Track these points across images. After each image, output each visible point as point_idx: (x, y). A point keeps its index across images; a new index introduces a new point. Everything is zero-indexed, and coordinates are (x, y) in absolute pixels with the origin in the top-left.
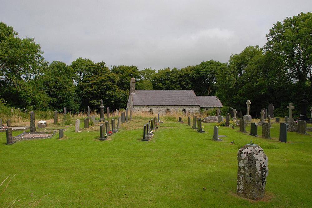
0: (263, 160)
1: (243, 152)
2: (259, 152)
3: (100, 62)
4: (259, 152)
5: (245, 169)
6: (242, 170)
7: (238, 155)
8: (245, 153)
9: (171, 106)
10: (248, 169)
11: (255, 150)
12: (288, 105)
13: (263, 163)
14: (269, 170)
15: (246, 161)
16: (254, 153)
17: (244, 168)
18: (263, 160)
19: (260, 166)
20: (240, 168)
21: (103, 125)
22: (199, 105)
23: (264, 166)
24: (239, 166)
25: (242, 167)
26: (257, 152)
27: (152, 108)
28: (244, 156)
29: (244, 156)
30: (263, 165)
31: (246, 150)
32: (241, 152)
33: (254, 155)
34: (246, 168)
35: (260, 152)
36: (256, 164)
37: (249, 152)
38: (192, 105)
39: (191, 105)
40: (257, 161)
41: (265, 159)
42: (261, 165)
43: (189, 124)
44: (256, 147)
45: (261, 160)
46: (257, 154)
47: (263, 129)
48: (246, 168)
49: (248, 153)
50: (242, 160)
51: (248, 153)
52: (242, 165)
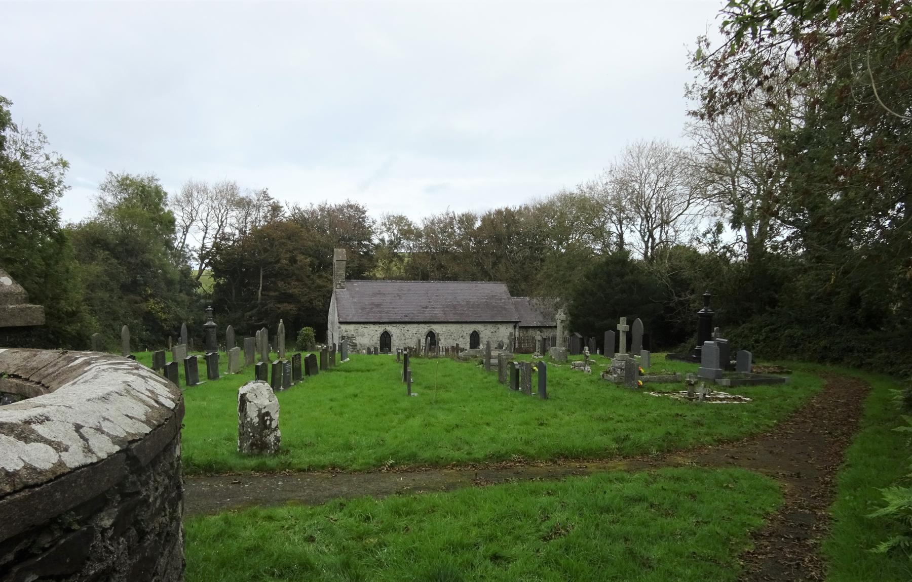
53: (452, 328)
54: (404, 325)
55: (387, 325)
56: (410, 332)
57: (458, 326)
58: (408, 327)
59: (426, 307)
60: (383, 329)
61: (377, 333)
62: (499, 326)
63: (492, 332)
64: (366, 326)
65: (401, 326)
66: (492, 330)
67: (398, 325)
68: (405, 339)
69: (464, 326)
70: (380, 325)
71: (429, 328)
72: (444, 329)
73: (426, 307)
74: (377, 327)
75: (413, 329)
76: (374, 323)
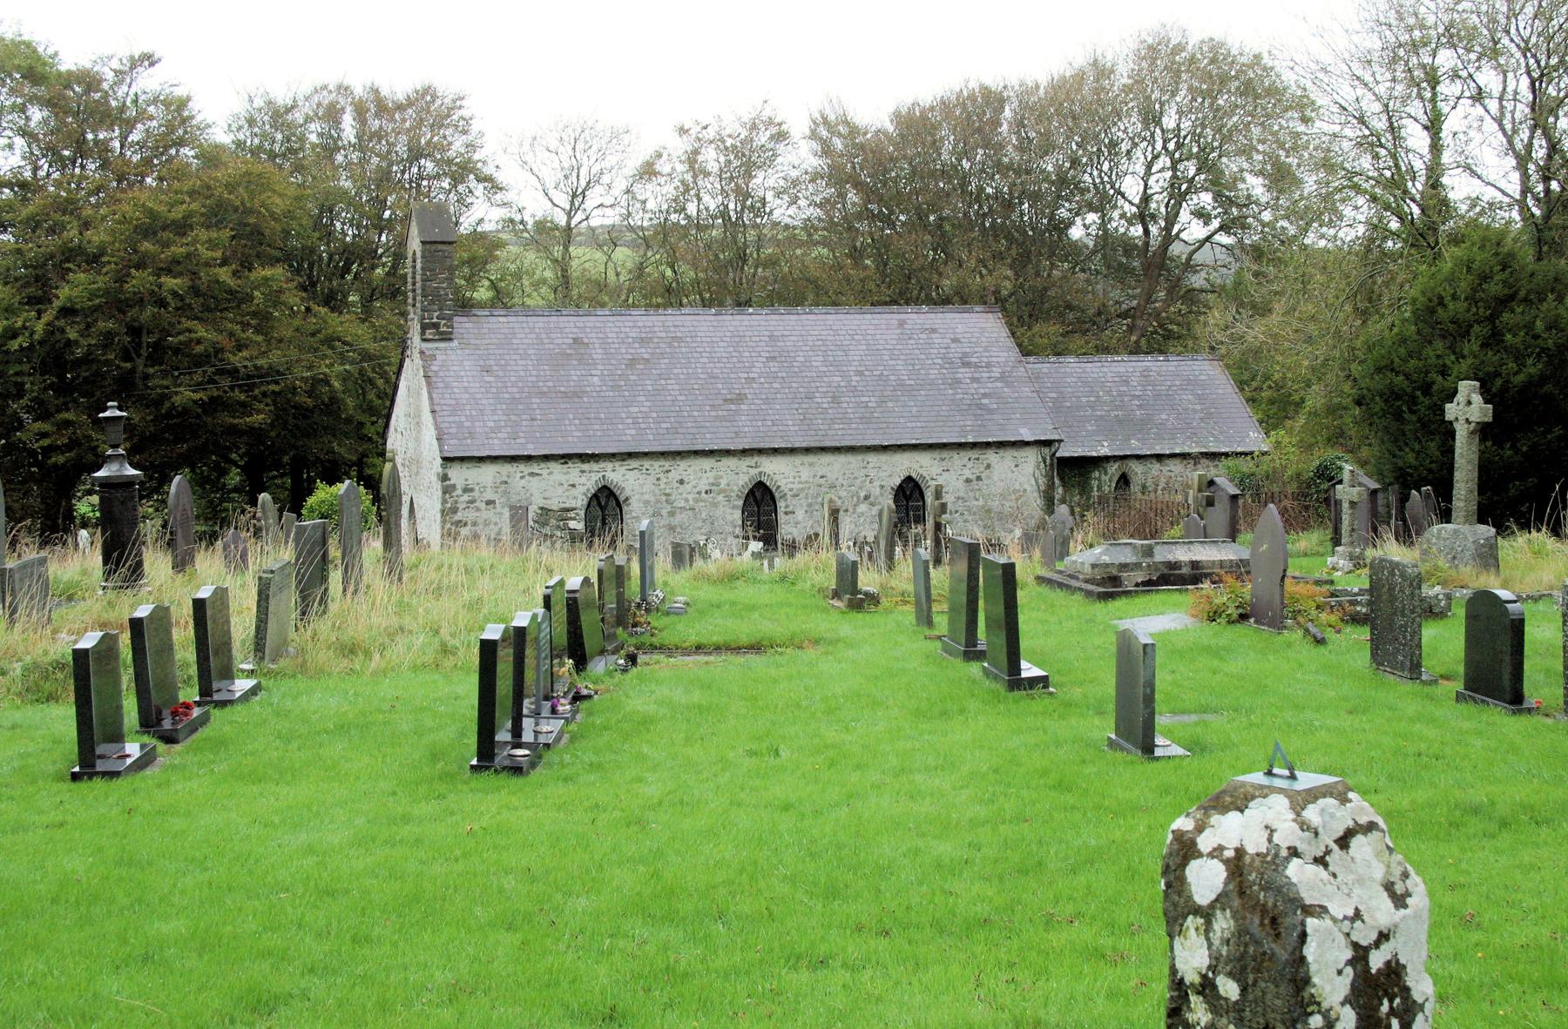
0: (1382, 912)
1: (1205, 842)
2: (1344, 842)
3: (1081, 60)
4: (1344, 842)
5: (1219, 997)
6: (1194, 999)
7: (1166, 871)
8: (1217, 852)
9: (792, 451)
10: (1244, 990)
11: (1304, 826)
12: (1451, 395)
13: (1383, 937)
14: (1442, 999)
15: (1223, 924)
16: (1294, 852)
17: (1207, 987)
18: (1382, 912)
19: (1350, 962)
20: (1178, 985)
21: (108, 646)
22: (1047, 443)
23: (1394, 970)
24: (1173, 970)
25: (1197, 980)
26: (1328, 839)
27: (618, 476)
28: (1206, 880)
29: (1206, 880)
30: (1377, 961)
31: (1229, 830)
32: (1185, 849)
33: (1297, 871)
34: (1229, 989)
35: (1358, 842)
36: (1310, 951)
37: (1255, 844)
38: (988, 445)
39: (974, 445)
40: (1311, 922)
41: (1400, 900)
42: (1360, 955)
43: (926, 619)
44: (1313, 795)
45: (1357, 915)
46: (1320, 861)
47: (569, 632)
48: (1229, 989)
49: (1240, 852)
50: (1197, 911)
51: (1240, 852)
52: (1193, 957)
53: (833, 466)
54: (667, 464)
55: (609, 465)
56: (688, 487)
57: (854, 460)
58: (683, 468)
59: (740, 398)
60: (595, 477)
61: (574, 492)
62: (991, 456)
63: (968, 481)
64: (535, 468)
65: (656, 466)
66: (967, 474)
67: (647, 463)
68: (672, 514)
69: (873, 458)
70: (586, 467)
71: (754, 472)
72: (805, 474)
73: (740, 398)
74: (574, 471)
75: (698, 473)
76: (566, 458)
